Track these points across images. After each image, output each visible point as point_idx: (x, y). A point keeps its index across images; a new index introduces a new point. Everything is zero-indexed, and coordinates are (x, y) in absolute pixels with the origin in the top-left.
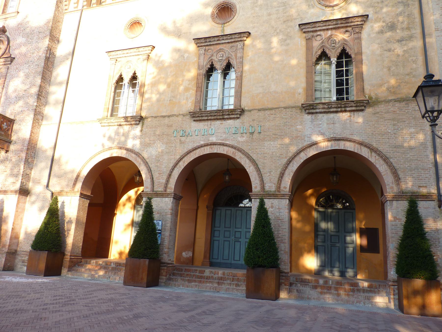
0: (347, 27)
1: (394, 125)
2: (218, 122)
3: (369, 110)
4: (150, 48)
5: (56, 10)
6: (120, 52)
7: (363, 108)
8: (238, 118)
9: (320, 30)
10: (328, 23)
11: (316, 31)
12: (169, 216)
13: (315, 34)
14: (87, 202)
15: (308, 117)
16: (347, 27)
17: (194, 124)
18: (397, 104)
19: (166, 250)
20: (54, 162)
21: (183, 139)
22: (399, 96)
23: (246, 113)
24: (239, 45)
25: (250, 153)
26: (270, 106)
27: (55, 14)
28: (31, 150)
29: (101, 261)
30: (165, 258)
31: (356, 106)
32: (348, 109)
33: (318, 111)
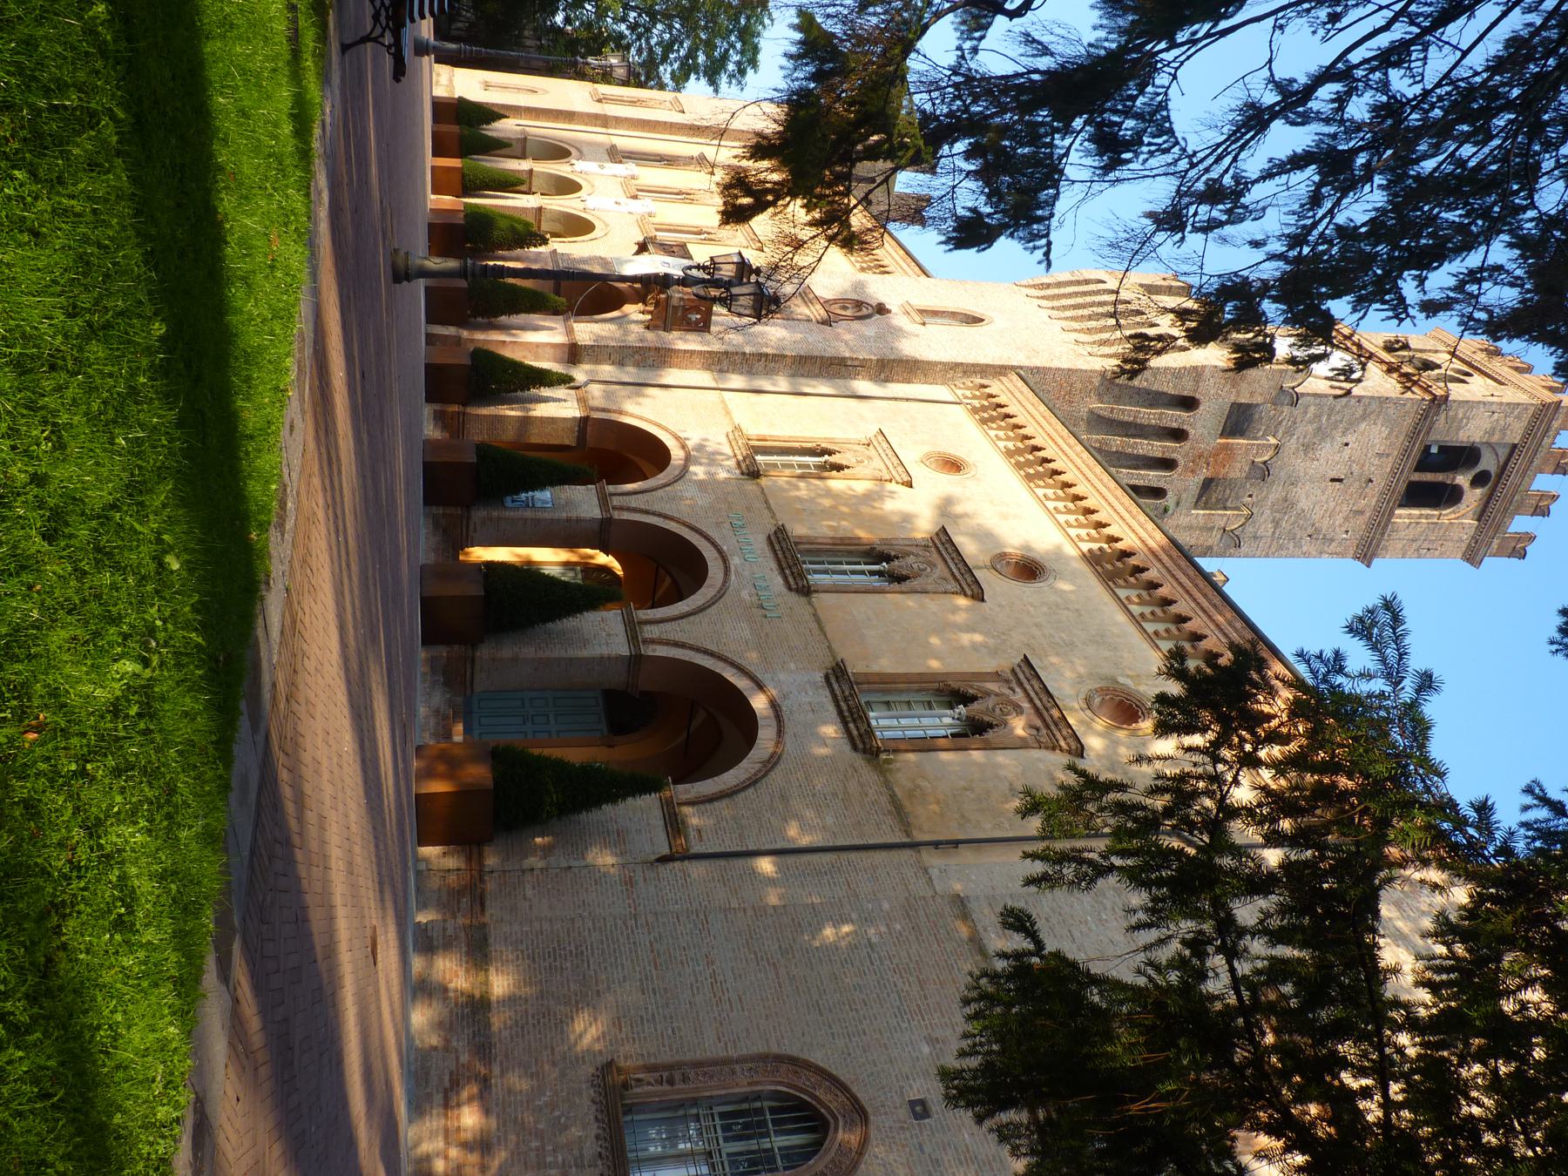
0: (1048, 727)
1: (835, 795)
2: (774, 565)
3: (859, 760)
4: (906, 478)
5: (944, 364)
6: (885, 445)
7: (860, 746)
8: (790, 589)
9: (1025, 690)
10: (1043, 696)
11: (1021, 684)
12: (564, 515)
13: (1014, 685)
14: (569, 440)
15: (819, 677)
16: (1048, 727)
17: (762, 538)
18: (884, 800)
19: (495, 514)
20: (722, 862)
21: (727, 525)
22: (906, 803)
23: (803, 600)
24: (953, 586)
25: (720, 604)
26: (828, 629)
27: (936, 364)
28: (660, 358)
29: (494, 1011)
30: (484, 652)
31: (860, 735)
32: (851, 726)
33: (836, 686)
